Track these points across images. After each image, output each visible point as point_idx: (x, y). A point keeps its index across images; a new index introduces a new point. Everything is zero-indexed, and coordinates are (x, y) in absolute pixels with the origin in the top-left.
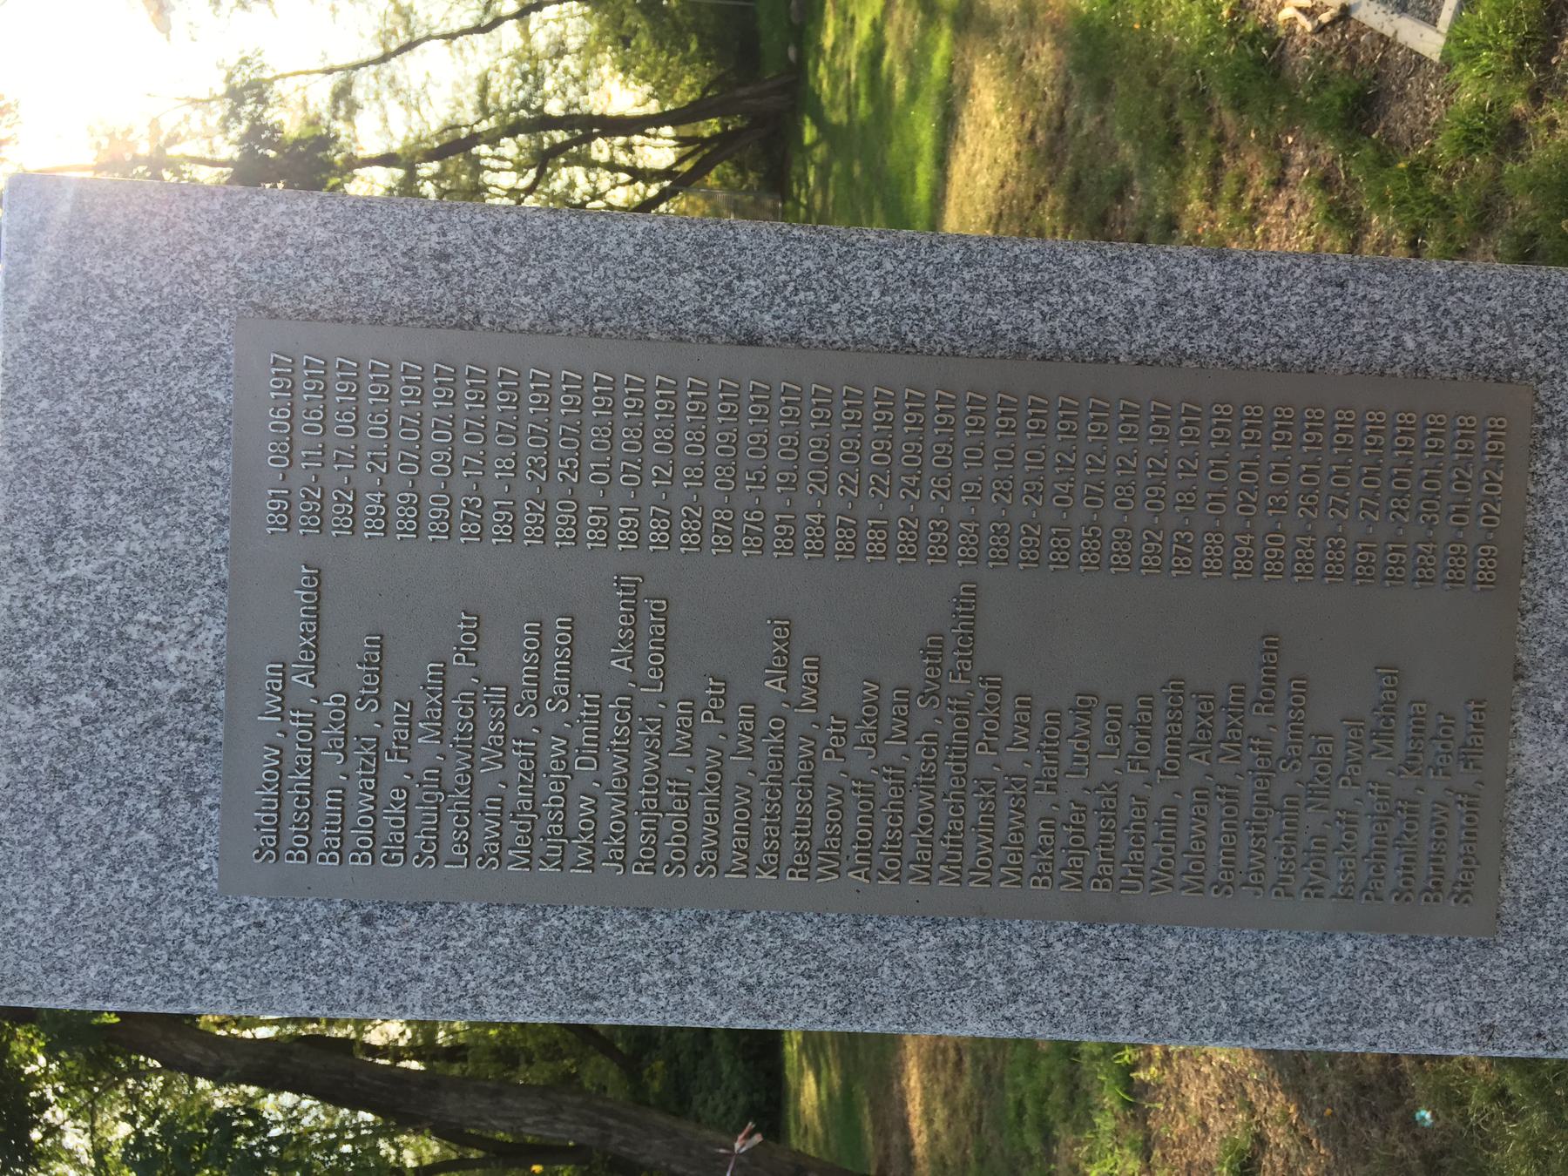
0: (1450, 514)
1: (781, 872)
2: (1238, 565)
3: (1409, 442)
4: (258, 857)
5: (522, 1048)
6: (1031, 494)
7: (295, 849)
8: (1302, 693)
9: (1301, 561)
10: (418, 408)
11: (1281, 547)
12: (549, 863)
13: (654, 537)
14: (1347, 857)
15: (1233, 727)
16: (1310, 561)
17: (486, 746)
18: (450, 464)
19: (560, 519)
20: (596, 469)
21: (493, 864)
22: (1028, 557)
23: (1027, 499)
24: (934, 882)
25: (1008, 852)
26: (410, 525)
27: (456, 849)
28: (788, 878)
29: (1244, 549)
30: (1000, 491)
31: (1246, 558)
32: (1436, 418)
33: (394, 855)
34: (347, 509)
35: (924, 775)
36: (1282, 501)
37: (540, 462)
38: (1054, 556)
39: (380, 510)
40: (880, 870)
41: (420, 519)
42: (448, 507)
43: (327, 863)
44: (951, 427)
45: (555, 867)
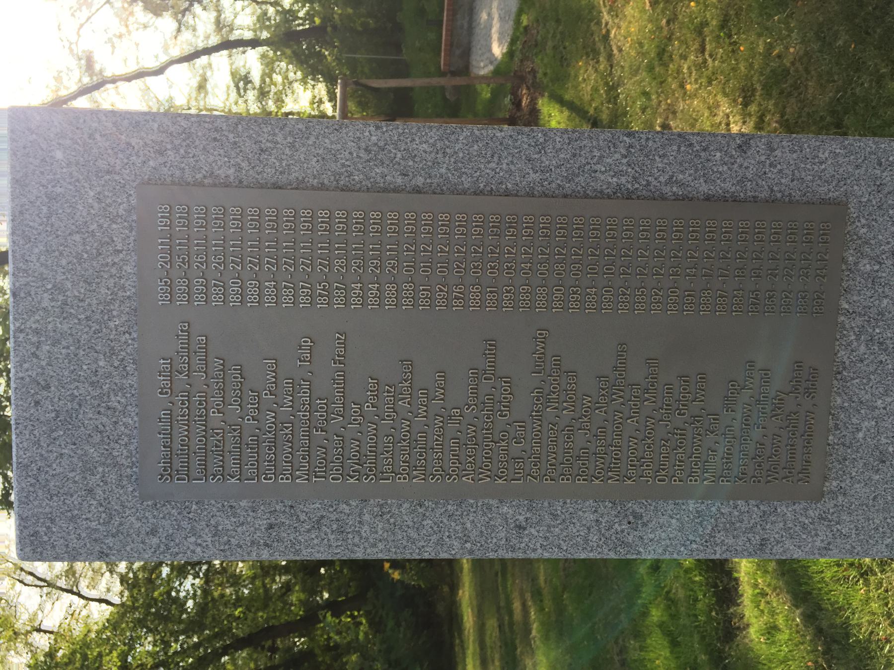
1: (360, 478)
4: (160, 479)
11: (677, 296)
12: (352, 478)
16: (644, 303)
17: (333, 414)
19: (232, 291)
25: (564, 468)
27: (198, 472)
28: (720, 483)
29: (357, 291)
30: (339, 266)
31: (576, 301)
32: (825, 225)
33: (269, 476)
34: (444, 295)
39: (377, 294)
40: (228, 475)
41: (295, 296)
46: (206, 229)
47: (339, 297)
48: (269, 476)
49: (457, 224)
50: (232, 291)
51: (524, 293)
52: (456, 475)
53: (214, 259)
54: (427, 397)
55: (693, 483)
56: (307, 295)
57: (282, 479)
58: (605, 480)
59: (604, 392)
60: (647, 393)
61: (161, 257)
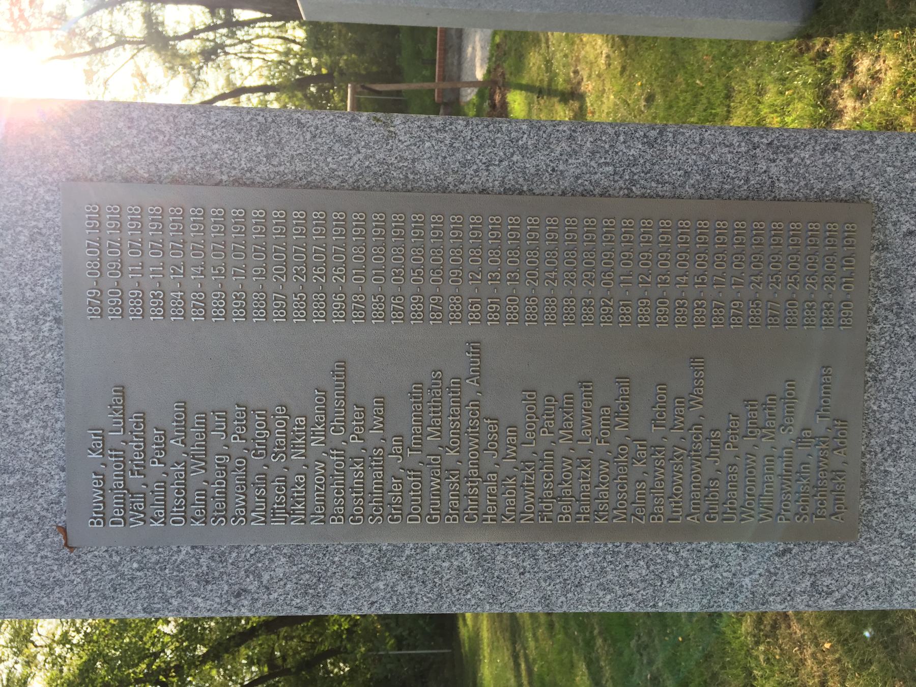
0: (842, 284)
2: (678, 319)
3: (724, 240)
5: (725, 613)
6: (587, 280)
7: (451, 515)
8: (664, 394)
9: (623, 314)
10: (223, 239)
12: (197, 520)
13: (256, 313)
14: (604, 490)
15: (567, 420)
16: (629, 314)
18: (120, 270)
20: (376, 274)
21: (242, 521)
22: (681, 321)
23: (585, 283)
24: (308, 522)
26: (138, 311)
32: (721, 223)
33: (434, 517)
35: (695, 451)
36: (516, 276)
37: (302, 270)
38: (752, 320)
42: (120, 298)
43: (336, 523)
44: (499, 239)
45: (511, 520)
46: (121, 232)
47: (512, 313)
48: (434, 517)
49: (432, 226)
50: (335, 306)
51: (416, 303)
52: (381, 515)
53: (433, 273)
54: (421, 426)
55: (95, 526)
56: (241, 308)
57: (333, 520)
58: (610, 519)
59: (568, 416)
60: (617, 417)
61: (276, 270)
